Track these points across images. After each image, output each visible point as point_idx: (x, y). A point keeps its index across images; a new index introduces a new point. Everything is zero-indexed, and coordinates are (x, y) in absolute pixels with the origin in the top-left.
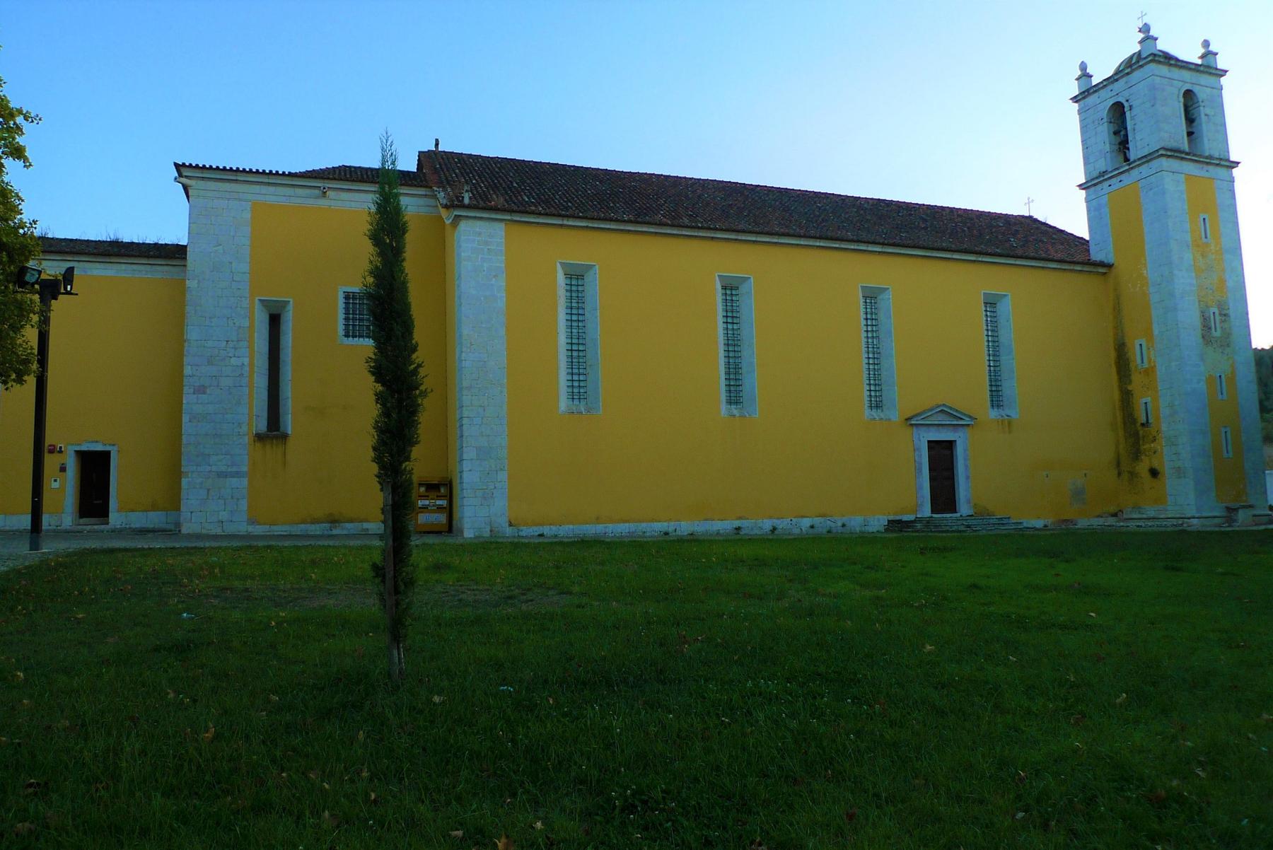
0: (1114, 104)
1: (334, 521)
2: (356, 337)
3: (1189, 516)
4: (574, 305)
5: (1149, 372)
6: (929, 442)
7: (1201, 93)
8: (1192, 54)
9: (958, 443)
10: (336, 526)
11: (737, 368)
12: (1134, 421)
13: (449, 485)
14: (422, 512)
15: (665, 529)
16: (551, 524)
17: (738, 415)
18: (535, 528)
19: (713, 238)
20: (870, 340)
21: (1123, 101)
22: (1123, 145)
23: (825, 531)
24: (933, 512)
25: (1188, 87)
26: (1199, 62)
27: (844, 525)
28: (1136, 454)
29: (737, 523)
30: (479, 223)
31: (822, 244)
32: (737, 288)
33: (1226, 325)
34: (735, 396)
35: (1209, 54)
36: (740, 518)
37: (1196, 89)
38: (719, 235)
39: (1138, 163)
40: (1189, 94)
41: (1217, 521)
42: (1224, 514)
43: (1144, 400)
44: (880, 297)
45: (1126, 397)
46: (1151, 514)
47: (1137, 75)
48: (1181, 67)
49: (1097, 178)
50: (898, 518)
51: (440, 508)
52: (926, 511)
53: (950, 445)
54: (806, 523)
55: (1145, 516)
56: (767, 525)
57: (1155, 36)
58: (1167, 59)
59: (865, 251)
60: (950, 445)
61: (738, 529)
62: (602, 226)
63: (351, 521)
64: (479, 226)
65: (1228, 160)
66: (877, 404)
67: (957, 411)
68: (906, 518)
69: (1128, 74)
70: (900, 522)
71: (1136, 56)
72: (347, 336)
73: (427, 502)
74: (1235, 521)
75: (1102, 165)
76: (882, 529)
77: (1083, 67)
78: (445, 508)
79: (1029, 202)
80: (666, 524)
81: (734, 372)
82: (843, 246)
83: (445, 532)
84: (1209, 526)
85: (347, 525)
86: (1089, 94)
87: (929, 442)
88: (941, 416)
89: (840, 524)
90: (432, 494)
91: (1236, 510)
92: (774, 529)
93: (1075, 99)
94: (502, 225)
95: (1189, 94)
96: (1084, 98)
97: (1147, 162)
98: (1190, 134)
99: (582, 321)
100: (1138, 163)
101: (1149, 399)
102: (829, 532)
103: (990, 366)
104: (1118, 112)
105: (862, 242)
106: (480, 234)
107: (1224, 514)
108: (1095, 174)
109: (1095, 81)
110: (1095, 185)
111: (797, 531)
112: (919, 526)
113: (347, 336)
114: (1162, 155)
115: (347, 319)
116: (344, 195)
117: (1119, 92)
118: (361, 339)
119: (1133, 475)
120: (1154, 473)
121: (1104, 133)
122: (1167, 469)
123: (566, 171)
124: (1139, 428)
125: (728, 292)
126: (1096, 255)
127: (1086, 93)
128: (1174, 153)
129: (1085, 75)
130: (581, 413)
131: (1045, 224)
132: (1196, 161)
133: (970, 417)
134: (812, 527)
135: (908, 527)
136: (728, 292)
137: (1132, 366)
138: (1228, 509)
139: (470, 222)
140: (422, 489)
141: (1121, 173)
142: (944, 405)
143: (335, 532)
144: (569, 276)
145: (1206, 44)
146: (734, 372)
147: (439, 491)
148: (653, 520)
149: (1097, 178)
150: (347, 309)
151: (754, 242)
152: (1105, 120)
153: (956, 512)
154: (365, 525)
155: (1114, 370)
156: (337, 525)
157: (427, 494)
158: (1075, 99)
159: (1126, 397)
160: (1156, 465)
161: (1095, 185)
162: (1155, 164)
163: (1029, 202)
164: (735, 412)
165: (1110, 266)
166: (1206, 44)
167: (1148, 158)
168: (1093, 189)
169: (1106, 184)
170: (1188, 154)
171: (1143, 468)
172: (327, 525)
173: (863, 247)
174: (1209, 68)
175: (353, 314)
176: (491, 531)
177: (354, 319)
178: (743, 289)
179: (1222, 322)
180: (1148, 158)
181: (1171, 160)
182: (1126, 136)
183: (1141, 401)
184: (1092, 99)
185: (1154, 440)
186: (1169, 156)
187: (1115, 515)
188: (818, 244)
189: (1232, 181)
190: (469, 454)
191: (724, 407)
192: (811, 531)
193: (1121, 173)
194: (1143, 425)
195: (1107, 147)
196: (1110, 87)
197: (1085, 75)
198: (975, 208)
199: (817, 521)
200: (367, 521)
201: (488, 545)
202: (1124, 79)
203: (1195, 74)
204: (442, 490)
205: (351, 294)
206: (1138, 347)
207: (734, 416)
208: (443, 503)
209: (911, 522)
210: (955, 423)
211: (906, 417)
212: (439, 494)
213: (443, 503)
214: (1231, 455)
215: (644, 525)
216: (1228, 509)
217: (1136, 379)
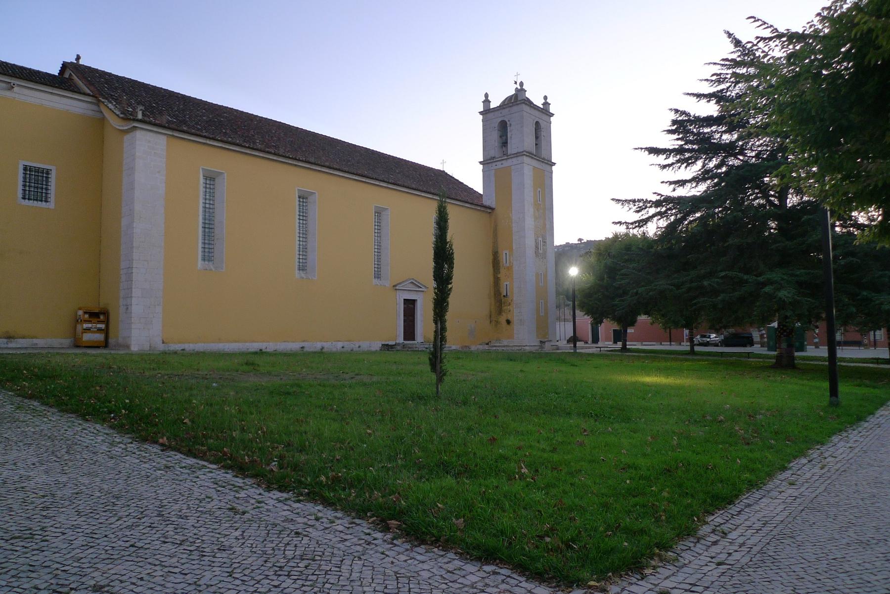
0: (502, 121)
1: (10, 337)
2: (31, 199)
3: (524, 345)
4: (207, 197)
5: (510, 268)
6: (404, 299)
7: (542, 124)
8: (539, 102)
9: (418, 301)
10: (11, 341)
11: (305, 249)
12: (500, 294)
13: (106, 313)
14: (85, 332)
15: (260, 348)
16: (189, 343)
17: (305, 277)
18: (179, 345)
19: (296, 165)
20: (301, 225)
21: (507, 120)
22: (505, 144)
23: (349, 350)
24: (405, 339)
25: (537, 120)
26: (542, 107)
27: (359, 347)
28: (500, 311)
29: (302, 344)
30: (151, 134)
31: (356, 178)
32: (307, 198)
33: (545, 248)
34: (302, 268)
35: (546, 104)
36: (304, 341)
37: (540, 122)
38: (300, 164)
39: (512, 156)
40: (537, 123)
41: (537, 348)
42: (539, 344)
43: (505, 283)
44: (384, 213)
45: (497, 281)
46: (505, 344)
47: (515, 108)
48: (535, 109)
49: (490, 160)
50: (387, 343)
51: (100, 330)
52: (401, 340)
53: (413, 302)
54: (340, 345)
55: (502, 345)
56: (318, 345)
57: (549, 102)
58: (529, 102)
59: (378, 185)
60: (413, 302)
61: (303, 348)
62: (231, 148)
63: (24, 337)
64: (151, 137)
65: (551, 162)
66: (378, 276)
67: (419, 283)
68: (391, 343)
69: (511, 106)
70: (387, 345)
71: (513, 97)
72: (24, 198)
73: (90, 325)
74: (544, 348)
75: (492, 153)
76: (378, 349)
77: (486, 95)
78: (103, 330)
79: (443, 162)
80: (261, 344)
81: (304, 250)
82: (367, 181)
83: (102, 347)
84: (533, 349)
85: (20, 340)
86: (489, 112)
87: (404, 299)
88: (411, 285)
89: (357, 346)
90: (95, 320)
91: (544, 342)
92: (323, 348)
93: (481, 113)
94: (165, 138)
95: (537, 123)
96: (486, 113)
97: (517, 156)
98: (536, 144)
99: (212, 209)
100: (512, 156)
101: (508, 283)
102: (352, 350)
103: (300, 241)
104: (503, 127)
105: (377, 180)
106: (149, 142)
107: (539, 344)
108: (489, 157)
109: (492, 106)
110: (488, 163)
111: (334, 350)
112: (399, 348)
113: (24, 198)
114: (524, 155)
115: (24, 186)
116: (26, 92)
117: (505, 115)
118: (35, 202)
119: (497, 322)
120: (508, 322)
121: (495, 135)
122: (515, 320)
123: (292, 129)
124: (502, 298)
125: (301, 200)
126: (486, 202)
127: (487, 112)
128: (530, 155)
129: (487, 101)
130: (211, 270)
131: (452, 177)
132: (537, 160)
133: (425, 287)
134: (343, 347)
135: (392, 348)
136: (301, 200)
137: (501, 264)
138: (541, 342)
139: (143, 132)
140: (87, 316)
141: (503, 160)
142: (413, 279)
143: (10, 345)
144: (206, 178)
145: (545, 98)
146: (304, 250)
147: (99, 318)
148: (253, 341)
149: (490, 160)
150: (25, 178)
151: (319, 171)
152: (496, 128)
153: (414, 340)
154: (35, 341)
155: (491, 265)
156: (12, 340)
157: (91, 319)
158: (481, 113)
159: (497, 281)
160: (509, 318)
161: (488, 163)
162: (520, 158)
163: (443, 162)
164: (303, 275)
165: (493, 209)
166: (545, 98)
167: (518, 155)
168: (486, 165)
169: (494, 164)
170: (535, 156)
171: (503, 319)
172: (5, 340)
173: (377, 183)
174: (545, 111)
175: (29, 182)
176: (150, 347)
177: (29, 186)
178: (310, 199)
179: (544, 245)
180: (518, 155)
181: (528, 158)
182: (507, 139)
183: (504, 283)
184: (490, 115)
185: (510, 304)
186: (527, 156)
187: (487, 344)
188: (354, 178)
189: (552, 173)
190: (136, 292)
191: (200, 263)
192: (342, 350)
193: (503, 160)
194: (504, 296)
195: (496, 144)
196: (501, 111)
197: (487, 101)
198: (428, 166)
199: (346, 344)
200: (36, 338)
201: (143, 356)
202: (508, 109)
203: (541, 114)
204: (102, 317)
205: (28, 167)
206: (504, 255)
207: (303, 278)
208: (103, 326)
209: (394, 345)
210: (417, 289)
211: (394, 284)
212: (99, 320)
213: (103, 326)
214: (543, 314)
215: (247, 344)
216: (541, 342)
217: (503, 271)
